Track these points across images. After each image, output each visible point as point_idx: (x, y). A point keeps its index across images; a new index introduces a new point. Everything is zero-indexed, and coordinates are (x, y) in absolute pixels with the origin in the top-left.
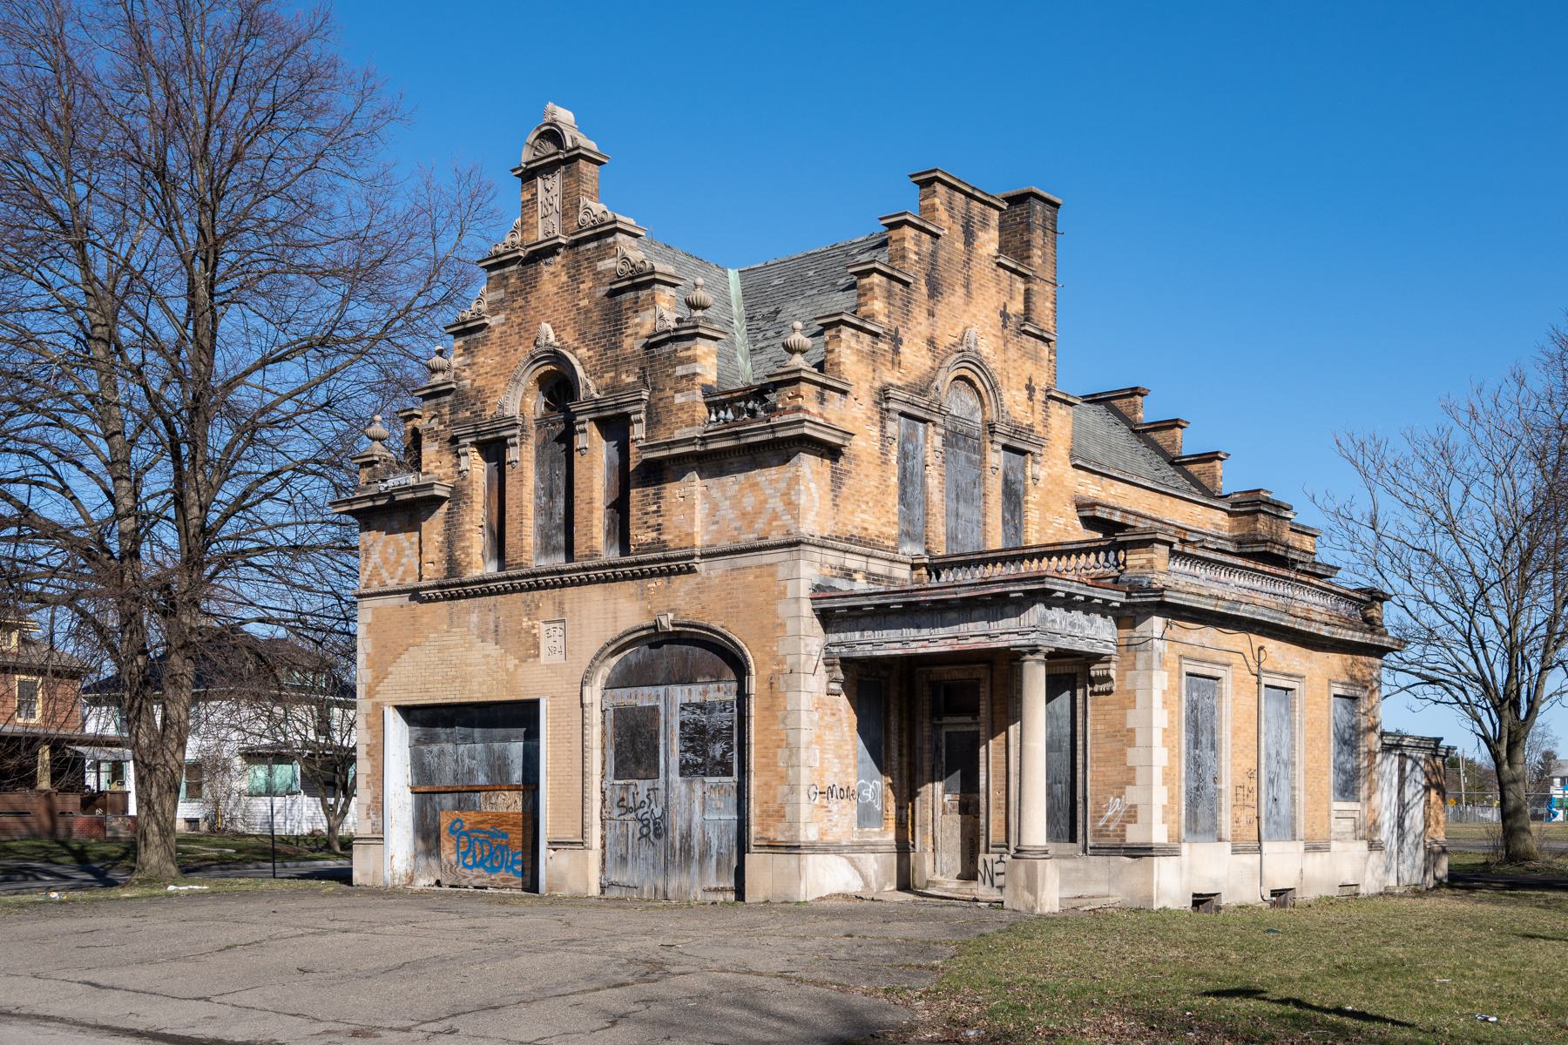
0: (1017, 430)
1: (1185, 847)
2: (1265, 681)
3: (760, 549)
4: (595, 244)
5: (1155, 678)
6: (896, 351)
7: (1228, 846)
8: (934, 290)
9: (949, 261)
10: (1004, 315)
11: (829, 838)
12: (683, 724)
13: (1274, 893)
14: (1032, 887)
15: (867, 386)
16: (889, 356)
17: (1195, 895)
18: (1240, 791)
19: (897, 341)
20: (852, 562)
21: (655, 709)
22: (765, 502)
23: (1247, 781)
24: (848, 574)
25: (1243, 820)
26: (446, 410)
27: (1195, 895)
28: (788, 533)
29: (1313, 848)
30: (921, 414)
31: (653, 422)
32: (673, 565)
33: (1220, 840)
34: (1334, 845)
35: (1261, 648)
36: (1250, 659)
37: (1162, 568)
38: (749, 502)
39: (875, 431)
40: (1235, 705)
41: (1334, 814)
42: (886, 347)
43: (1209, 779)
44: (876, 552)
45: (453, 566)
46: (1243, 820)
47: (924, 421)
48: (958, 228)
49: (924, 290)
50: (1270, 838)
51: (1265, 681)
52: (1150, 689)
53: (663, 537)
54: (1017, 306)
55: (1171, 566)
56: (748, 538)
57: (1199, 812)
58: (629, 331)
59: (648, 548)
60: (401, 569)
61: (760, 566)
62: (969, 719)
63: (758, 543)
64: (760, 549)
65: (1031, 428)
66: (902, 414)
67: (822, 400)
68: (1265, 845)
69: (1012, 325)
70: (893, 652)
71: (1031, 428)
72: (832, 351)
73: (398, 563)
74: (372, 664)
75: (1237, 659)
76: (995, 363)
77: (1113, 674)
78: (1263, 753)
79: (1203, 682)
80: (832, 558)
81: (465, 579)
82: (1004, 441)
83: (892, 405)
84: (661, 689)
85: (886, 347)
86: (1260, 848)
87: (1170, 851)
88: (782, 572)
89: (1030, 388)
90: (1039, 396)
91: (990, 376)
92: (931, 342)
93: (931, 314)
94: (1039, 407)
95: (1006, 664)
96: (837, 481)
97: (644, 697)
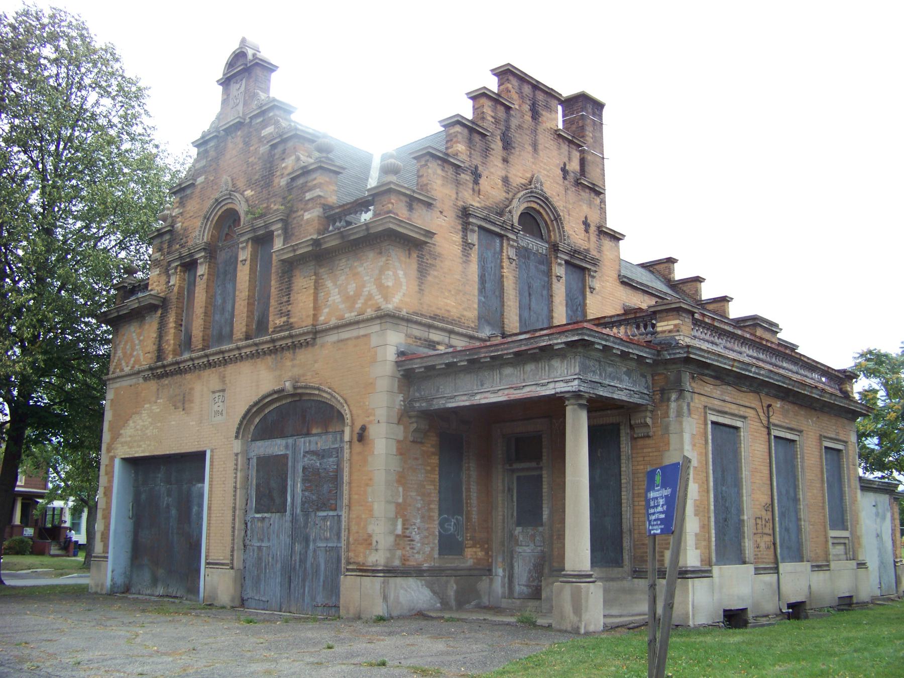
0: (574, 253)
1: (716, 570)
2: (774, 433)
3: (357, 323)
4: (261, 119)
5: (684, 424)
6: (476, 182)
7: (750, 568)
8: (507, 145)
9: (520, 127)
10: (564, 170)
11: (412, 563)
12: (304, 468)
13: (790, 606)
14: (578, 609)
15: (451, 204)
16: (471, 185)
17: (725, 611)
18: (759, 521)
19: (476, 176)
20: (435, 336)
21: (285, 456)
22: (364, 286)
23: (764, 513)
24: (432, 345)
25: (762, 545)
26: (165, 246)
27: (725, 611)
28: (379, 309)
29: (817, 568)
30: (497, 230)
31: (287, 233)
32: (296, 340)
33: (744, 563)
34: (833, 565)
35: (769, 406)
36: (761, 414)
37: (687, 333)
38: (351, 289)
39: (457, 238)
40: (754, 449)
41: (830, 541)
42: (468, 178)
43: (733, 511)
44: (456, 329)
45: (160, 354)
46: (762, 545)
47: (501, 236)
48: (526, 108)
49: (500, 144)
50: (783, 561)
51: (774, 433)
52: (681, 432)
53: (292, 320)
54: (574, 166)
55: (695, 333)
56: (350, 316)
57: (728, 544)
58: (278, 173)
59: (281, 329)
60: (133, 359)
61: (358, 338)
62: (534, 465)
63: (357, 318)
64: (357, 323)
65: (587, 251)
66: (480, 227)
67: (411, 208)
68: (782, 566)
69: (571, 177)
70: (462, 404)
71: (587, 251)
72: (422, 176)
73: (131, 355)
74: (111, 429)
75: (750, 413)
76: (559, 203)
77: (649, 421)
78: (775, 490)
79: (725, 436)
80: (417, 331)
81: (165, 362)
82: (567, 258)
83: (471, 220)
84: (290, 441)
85: (468, 178)
86: (776, 570)
87: (703, 573)
88: (374, 341)
89: (586, 224)
90: (593, 229)
91: (554, 210)
92: (506, 180)
93: (505, 160)
94: (593, 238)
95: (553, 408)
96: (423, 272)
97: (276, 447)
